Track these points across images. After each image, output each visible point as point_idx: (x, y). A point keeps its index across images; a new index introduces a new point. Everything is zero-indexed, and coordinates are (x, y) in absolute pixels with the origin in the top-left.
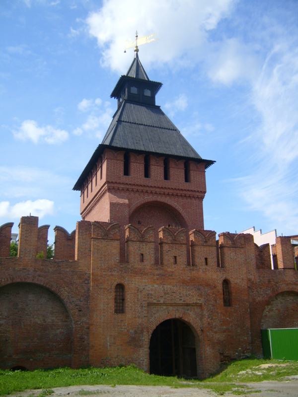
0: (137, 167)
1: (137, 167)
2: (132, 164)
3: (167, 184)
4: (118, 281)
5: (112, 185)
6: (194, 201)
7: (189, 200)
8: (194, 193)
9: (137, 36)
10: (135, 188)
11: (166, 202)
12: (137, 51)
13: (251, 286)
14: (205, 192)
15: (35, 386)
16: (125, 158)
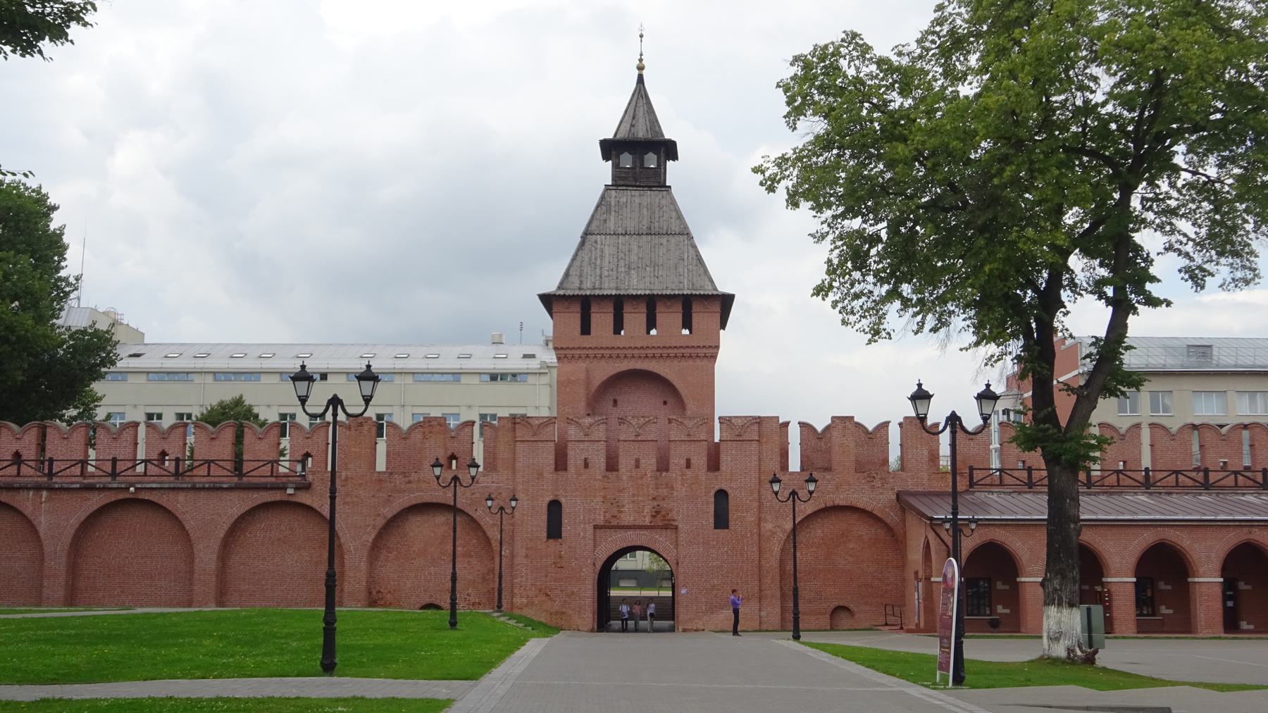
0: (602, 320)
1: (602, 320)
2: (593, 315)
3: (587, 341)
4: (550, 498)
5: (563, 352)
6: (698, 362)
7: (691, 362)
8: (698, 351)
9: (641, 36)
10: (629, 352)
11: (650, 369)
12: (641, 68)
13: (66, 279)
14: (717, 347)
15: (428, 601)
16: (582, 309)
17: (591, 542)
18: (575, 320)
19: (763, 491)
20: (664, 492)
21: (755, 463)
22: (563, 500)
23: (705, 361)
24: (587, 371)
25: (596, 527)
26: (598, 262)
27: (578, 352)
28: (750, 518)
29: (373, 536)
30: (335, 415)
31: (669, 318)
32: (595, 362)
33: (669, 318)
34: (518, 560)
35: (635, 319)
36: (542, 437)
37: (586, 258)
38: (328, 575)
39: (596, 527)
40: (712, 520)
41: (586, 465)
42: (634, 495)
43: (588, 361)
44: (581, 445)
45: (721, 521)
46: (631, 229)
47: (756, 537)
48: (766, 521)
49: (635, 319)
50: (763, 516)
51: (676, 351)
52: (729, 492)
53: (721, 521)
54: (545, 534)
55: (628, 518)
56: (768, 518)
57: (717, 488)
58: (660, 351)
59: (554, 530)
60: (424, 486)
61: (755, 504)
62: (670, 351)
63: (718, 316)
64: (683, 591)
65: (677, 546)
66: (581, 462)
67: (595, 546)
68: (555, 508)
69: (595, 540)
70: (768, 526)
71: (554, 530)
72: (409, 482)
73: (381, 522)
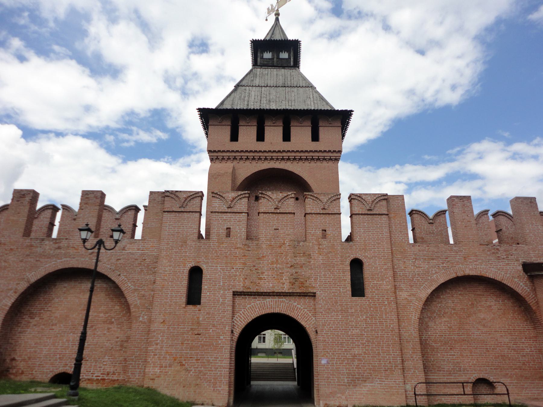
4: (193, 264)
12: (202, 404)
17: (230, 308)
18: (225, 132)
19: (396, 262)
20: (302, 260)
21: (386, 234)
22: (204, 267)
23: (331, 163)
24: (234, 168)
25: (235, 294)
26: (246, 98)
27: (228, 154)
28: (387, 285)
29: (13, 300)
30: (99, 249)
31: (301, 136)
32: (242, 162)
33: (301, 136)
34: (155, 326)
35: (274, 133)
36: (188, 209)
37: (238, 97)
38: (82, 333)
39: (235, 294)
40: (349, 288)
41: (228, 235)
42: (272, 263)
43: (235, 162)
44: (224, 216)
45: (358, 289)
46: (271, 83)
47: (394, 306)
48: (402, 290)
49: (274, 133)
50: (398, 284)
51: (307, 154)
52: (364, 260)
53: (358, 289)
54: (184, 299)
55: (266, 286)
56: (403, 286)
57: (352, 257)
58: (293, 154)
59: (194, 296)
60: (71, 251)
61: (390, 273)
62: (302, 154)
63: (340, 129)
64: (324, 362)
65: (315, 314)
66: (223, 232)
67: (233, 313)
68: (196, 274)
69: (233, 306)
70: (403, 295)
71: (194, 296)
72: (59, 248)
73: (23, 286)
